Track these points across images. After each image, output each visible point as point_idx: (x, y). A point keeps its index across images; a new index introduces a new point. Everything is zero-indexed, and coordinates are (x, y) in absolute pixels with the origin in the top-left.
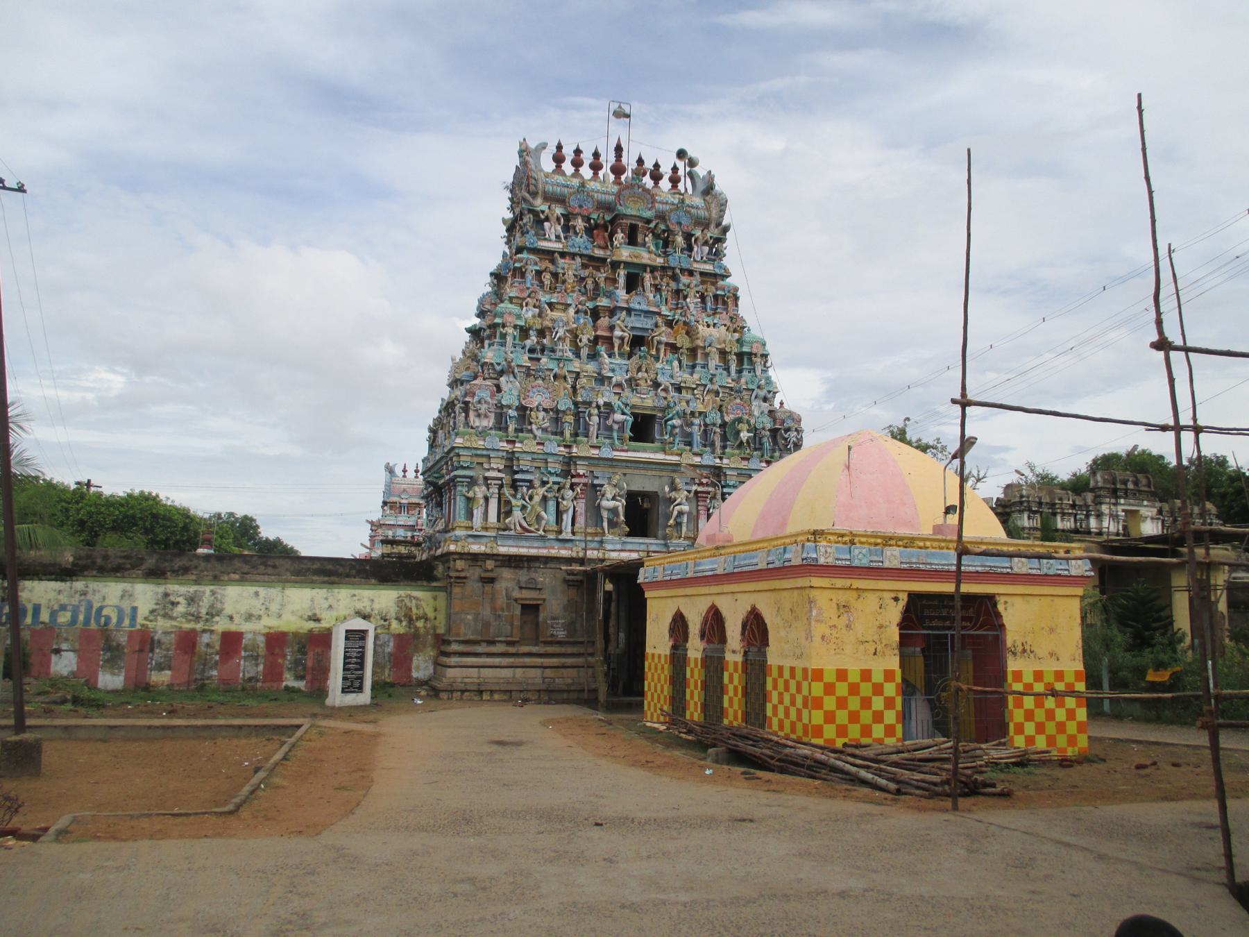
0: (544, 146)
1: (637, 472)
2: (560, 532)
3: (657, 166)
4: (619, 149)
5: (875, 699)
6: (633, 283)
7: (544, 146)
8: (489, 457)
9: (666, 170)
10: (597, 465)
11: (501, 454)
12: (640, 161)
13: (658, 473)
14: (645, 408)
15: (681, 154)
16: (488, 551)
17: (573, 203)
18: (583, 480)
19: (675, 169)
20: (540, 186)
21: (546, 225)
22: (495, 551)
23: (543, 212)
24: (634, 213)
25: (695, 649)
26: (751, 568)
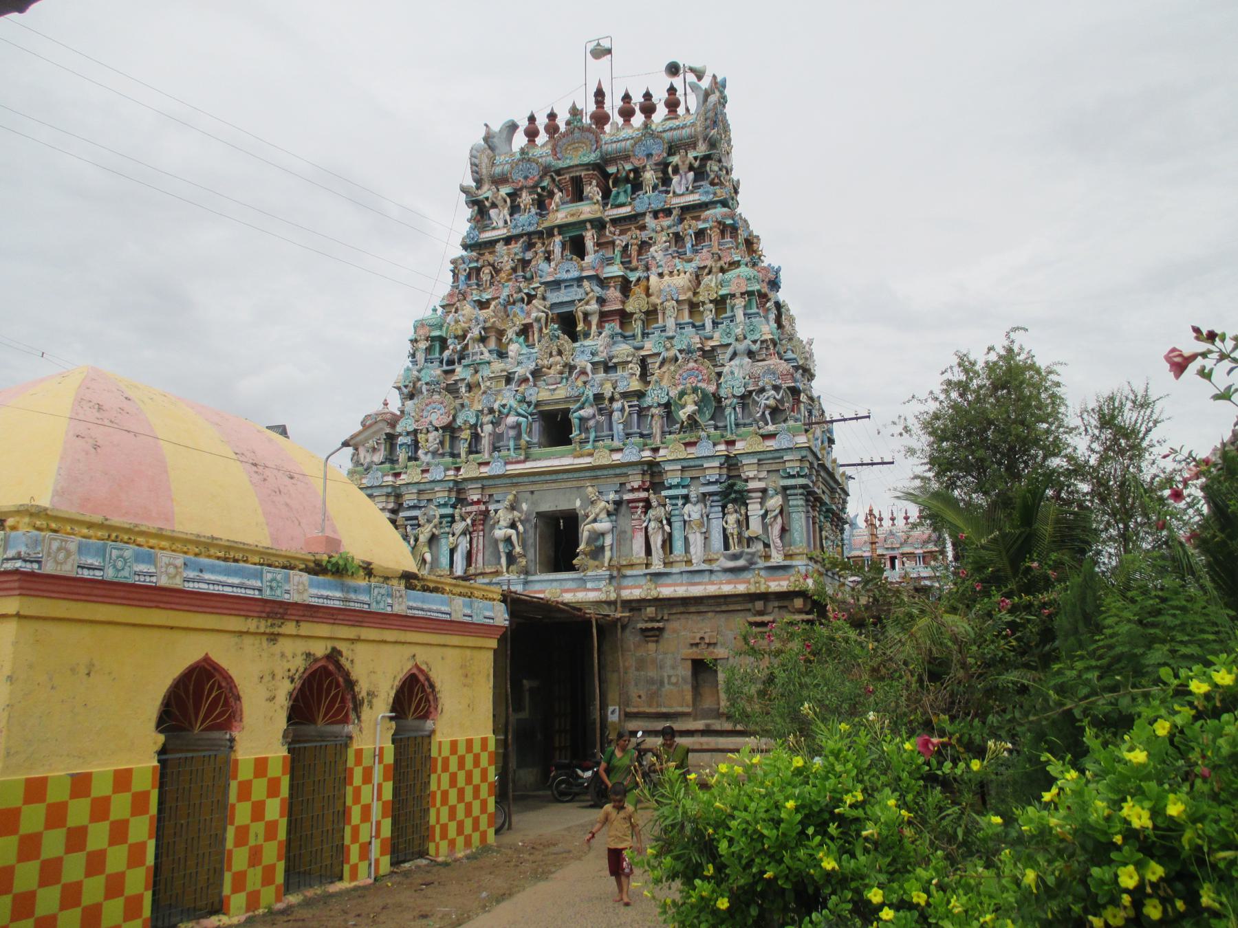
0: (513, 127)
1: (545, 486)
2: (648, 565)
3: (648, 96)
4: (600, 94)
5: (134, 822)
6: (577, 248)
7: (513, 127)
8: (626, 475)
9: (660, 96)
10: (495, 486)
11: (385, 490)
12: (627, 98)
13: (575, 484)
14: (557, 402)
15: (673, 69)
16: (753, 589)
17: (518, 177)
18: (475, 508)
19: (672, 90)
20: (484, 171)
21: (493, 212)
22: (763, 589)
23: (487, 199)
24: (576, 162)
25: (372, 734)
26: (420, 613)
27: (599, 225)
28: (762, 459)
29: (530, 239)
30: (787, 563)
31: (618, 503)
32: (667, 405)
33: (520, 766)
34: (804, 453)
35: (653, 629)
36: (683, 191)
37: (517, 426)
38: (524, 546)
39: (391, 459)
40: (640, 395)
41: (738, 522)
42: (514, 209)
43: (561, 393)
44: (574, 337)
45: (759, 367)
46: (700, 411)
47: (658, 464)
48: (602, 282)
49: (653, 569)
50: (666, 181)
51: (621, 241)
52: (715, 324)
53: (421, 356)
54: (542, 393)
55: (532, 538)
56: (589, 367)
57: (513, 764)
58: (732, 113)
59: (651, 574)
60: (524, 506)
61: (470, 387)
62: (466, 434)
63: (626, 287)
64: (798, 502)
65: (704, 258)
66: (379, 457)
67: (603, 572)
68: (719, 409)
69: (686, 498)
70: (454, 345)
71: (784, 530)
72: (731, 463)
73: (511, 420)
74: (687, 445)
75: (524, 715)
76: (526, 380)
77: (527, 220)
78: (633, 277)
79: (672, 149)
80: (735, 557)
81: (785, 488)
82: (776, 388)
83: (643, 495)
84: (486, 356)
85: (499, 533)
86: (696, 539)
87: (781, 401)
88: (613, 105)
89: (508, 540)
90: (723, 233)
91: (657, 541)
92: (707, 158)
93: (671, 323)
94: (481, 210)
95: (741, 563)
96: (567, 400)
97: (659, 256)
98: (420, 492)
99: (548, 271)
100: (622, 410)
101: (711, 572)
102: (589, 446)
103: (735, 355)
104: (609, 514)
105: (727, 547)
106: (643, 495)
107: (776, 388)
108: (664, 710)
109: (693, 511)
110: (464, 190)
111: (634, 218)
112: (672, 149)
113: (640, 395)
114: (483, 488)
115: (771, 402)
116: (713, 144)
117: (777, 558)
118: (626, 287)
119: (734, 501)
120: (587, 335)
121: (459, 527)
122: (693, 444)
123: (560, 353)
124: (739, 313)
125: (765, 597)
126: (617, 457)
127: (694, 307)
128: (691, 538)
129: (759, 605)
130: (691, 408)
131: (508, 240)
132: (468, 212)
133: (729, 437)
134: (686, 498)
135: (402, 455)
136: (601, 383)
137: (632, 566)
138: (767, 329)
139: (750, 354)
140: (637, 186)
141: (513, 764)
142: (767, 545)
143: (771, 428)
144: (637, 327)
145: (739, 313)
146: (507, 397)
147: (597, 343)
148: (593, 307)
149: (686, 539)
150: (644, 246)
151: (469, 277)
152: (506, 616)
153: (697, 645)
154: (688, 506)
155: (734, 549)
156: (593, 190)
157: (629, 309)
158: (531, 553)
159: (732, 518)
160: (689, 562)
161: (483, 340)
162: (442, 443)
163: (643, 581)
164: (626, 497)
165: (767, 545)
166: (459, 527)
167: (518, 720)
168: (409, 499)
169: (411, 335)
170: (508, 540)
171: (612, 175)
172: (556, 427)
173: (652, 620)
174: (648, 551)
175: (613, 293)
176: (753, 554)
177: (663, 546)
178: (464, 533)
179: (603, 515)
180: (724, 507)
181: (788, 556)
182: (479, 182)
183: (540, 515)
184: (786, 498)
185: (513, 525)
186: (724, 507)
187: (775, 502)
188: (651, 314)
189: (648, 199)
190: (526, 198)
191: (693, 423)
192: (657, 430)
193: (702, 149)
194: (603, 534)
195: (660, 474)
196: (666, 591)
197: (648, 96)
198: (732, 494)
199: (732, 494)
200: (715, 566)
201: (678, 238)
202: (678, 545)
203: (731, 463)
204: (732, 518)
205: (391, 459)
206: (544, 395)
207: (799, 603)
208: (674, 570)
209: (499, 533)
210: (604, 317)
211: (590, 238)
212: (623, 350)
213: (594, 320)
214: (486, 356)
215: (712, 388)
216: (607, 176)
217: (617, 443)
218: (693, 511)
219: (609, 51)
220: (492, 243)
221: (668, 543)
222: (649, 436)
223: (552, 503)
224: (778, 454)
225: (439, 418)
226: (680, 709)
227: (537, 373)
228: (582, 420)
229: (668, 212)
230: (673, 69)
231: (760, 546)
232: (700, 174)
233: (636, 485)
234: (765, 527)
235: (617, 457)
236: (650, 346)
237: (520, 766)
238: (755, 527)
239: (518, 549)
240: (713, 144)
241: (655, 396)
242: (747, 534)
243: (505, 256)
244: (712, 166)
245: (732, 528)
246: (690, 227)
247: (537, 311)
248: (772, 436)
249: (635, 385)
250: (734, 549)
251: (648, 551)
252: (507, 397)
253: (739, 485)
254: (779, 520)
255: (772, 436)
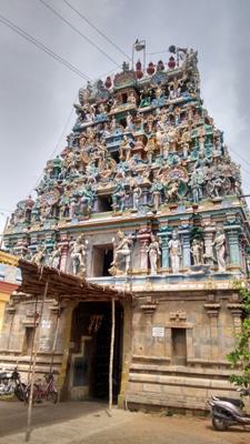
2: (148, 273)
6: (124, 123)
15: (172, 49)
16: (207, 288)
21: (87, 116)
22: (213, 288)
27: (133, 112)
28: (213, 215)
29: (102, 124)
30: (228, 272)
31: (135, 240)
32: (162, 191)
33: (74, 385)
34: (238, 211)
35: (149, 309)
36: (175, 97)
37: (86, 201)
38: (85, 262)
39: (28, 222)
40: (149, 187)
41: (199, 249)
42: (97, 112)
43: (109, 186)
44: (118, 161)
45: (212, 169)
46: (179, 191)
47: (156, 219)
48: (134, 138)
49: (151, 275)
50: (167, 94)
51: (144, 121)
52: (189, 154)
53: (48, 176)
54: (99, 187)
55: (89, 258)
56: (123, 173)
57: (71, 383)
58: (199, 66)
59: (151, 278)
60: (87, 242)
61: (68, 188)
62: (63, 208)
63: (145, 141)
64: (234, 241)
65: (184, 124)
66: (22, 220)
67: (125, 275)
68: (190, 190)
69: (170, 237)
70: (64, 171)
71: (226, 255)
72: (196, 218)
73: (83, 198)
74: (171, 208)
75: (81, 355)
76: (93, 181)
77: (103, 115)
78: (149, 137)
79: (171, 79)
80: (197, 269)
81: (226, 231)
82: (222, 177)
83: (148, 235)
84: (77, 173)
85: (73, 255)
86: (176, 260)
87: (224, 184)
88: (145, 66)
89: (77, 259)
90: (194, 112)
91: (154, 259)
92: (188, 81)
93: (166, 153)
94: (82, 115)
95: (201, 272)
96: (112, 189)
97: (162, 125)
98: (38, 236)
99: (107, 134)
100: (138, 192)
101: (183, 277)
102: (121, 211)
103: (198, 166)
104: (129, 246)
105: (192, 263)
106: (148, 235)
107: (222, 177)
108: (154, 357)
109: (174, 244)
110: (76, 106)
111: (152, 111)
112: (171, 79)
113: (149, 187)
114: (68, 233)
115: (219, 184)
116: (190, 74)
117: (222, 270)
118: (145, 141)
119: (197, 238)
120: (124, 161)
121: (55, 253)
122: (175, 208)
123: (110, 168)
124: (202, 146)
125: (214, 292)
126: (134, 215)
127: (178, 147)
128: (173, 258)
129: (211, 297)
130: (174, 189)
131: (93, 126)
132: (77, 116)
133: (195, 204)
134: (170, 237)
135: (33, 219)
136: (132, 181)
137: (140, 273)
138: (217, 153)
139: (207, 164)
140: (153, 97)
141: (71, 383)
142: (216, 263)
143: (218, 198)
144: (150, 157)
145: (202, 146)
146: (82, 189)
147: (130, 162)
148: (128, 146)
149: (170, 259)
150: (155, 122)
151: (74, 142)
152: (20, 278)
153: (174, 319)
154: (171, 241)
155: (197, 264)
156: (132, 98)
157: (146, 149)
158: (89, 267)
159: (196, 248)
160: (171, 272)
161: (77, 167)
162: (52, 213)
163: (144, 282)
164: (138, 236)
165: (216, 263)
166: (55, 253)
167: (76, 358)
168: (34, 239)
169: (45, 166)
170: (77, 259)
171: (144, 94)
172: (106, 203)
173: (149, 304)
174: (149, 267)
175: (140, 142)
176: (208, 267)
177: (157, 263)
178: (57, 256)
179: (126, 246)
180: (191, 242)
181: (228, 269)
182: (82, 103)
183: (95, 247)
184: (227, 236)
185: (81, 252)
186: (191, 242)
187: (221, 238)
188: (156, 151)
189: (158, 101)
190: (102, 107)
191: (175, 198)
192: (156, 202)
193: (185, 77)
194: (125, 256)
195: (157, 225)
196: (158, 287)
197: (160, 62)
198: (196, 234)
199: (196, 234)
200: (185, 274)
201: (172, 118)
202: (165, 263)
203: (196, 218)
204: (196, 248)
205: (28, 222)
206: (101, 188)
207: (235, 296)
208: (164, 275)
209: (73, 255)
210: (133, 153)
211: (129, 119)
212: (141, 166)
213: (128, 153)
214: (77, 173)
215: (186, 180)
216: (139, 94)
217: (135, 209)
218: (174, 244)
219: (143, 47)
220: (84, 129)
221: (160, 262)
222: (152, 207)
223: (101, 240)
224: (222, 213)
225: (51, 202)
226: (163, 358)
227: (98, 178)
228: (119, 198)
229: (167, 107)
230: (172, 49)
231: (212, 264)
232: (184, 89)
233: (144, 230)
234: (214, 251)
235: (134, 215)
236: (154, 165)
237: (74, 385)
238: (209, 253)
239: (82, 264)
240: (190, 74)
241: (157, 186)
242: (204, 256)
243: (91, 133)
244: (190, 85)
245: (196, 253)
246: (179, 111)
247: (102, 149)
248: (220, 202)
249: (146, 181)
250: (197, 264)
251: (149, 267)
252: (82, 189)
253: (200, 229)
254: (223, 248)
255: (220, 202)
